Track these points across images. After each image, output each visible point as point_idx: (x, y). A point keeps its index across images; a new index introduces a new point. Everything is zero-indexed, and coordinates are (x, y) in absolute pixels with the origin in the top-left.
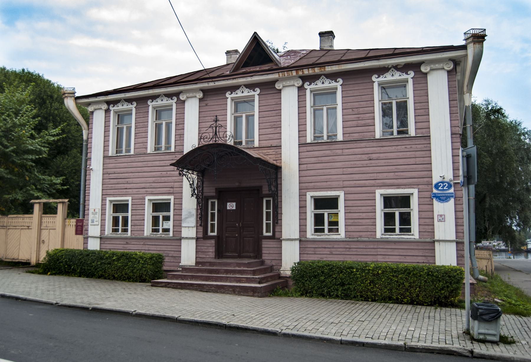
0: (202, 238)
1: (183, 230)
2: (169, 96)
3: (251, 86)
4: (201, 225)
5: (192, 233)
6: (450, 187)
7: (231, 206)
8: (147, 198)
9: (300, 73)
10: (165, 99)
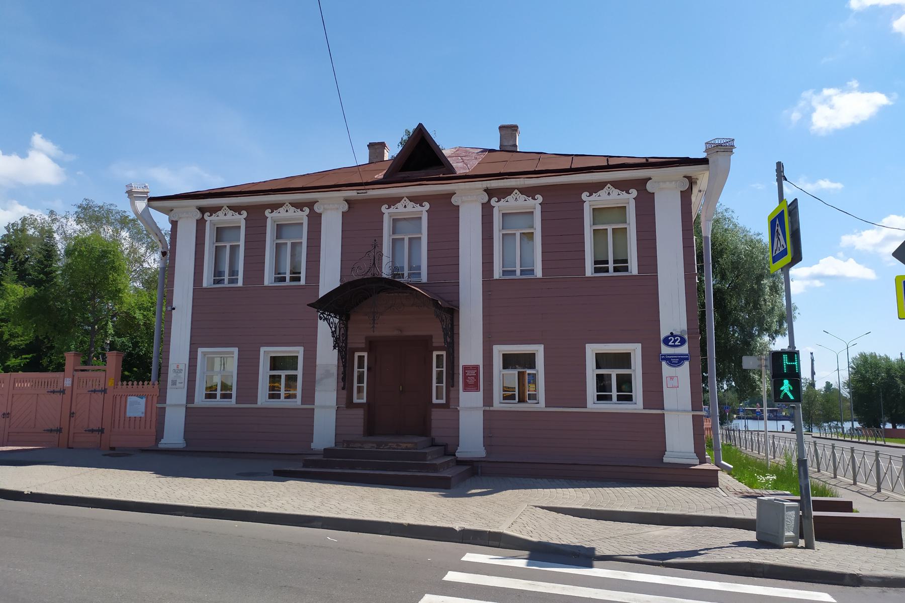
2: (299, 206)
3: (417, 199)
4: (343, 389)
10: (615, 192)
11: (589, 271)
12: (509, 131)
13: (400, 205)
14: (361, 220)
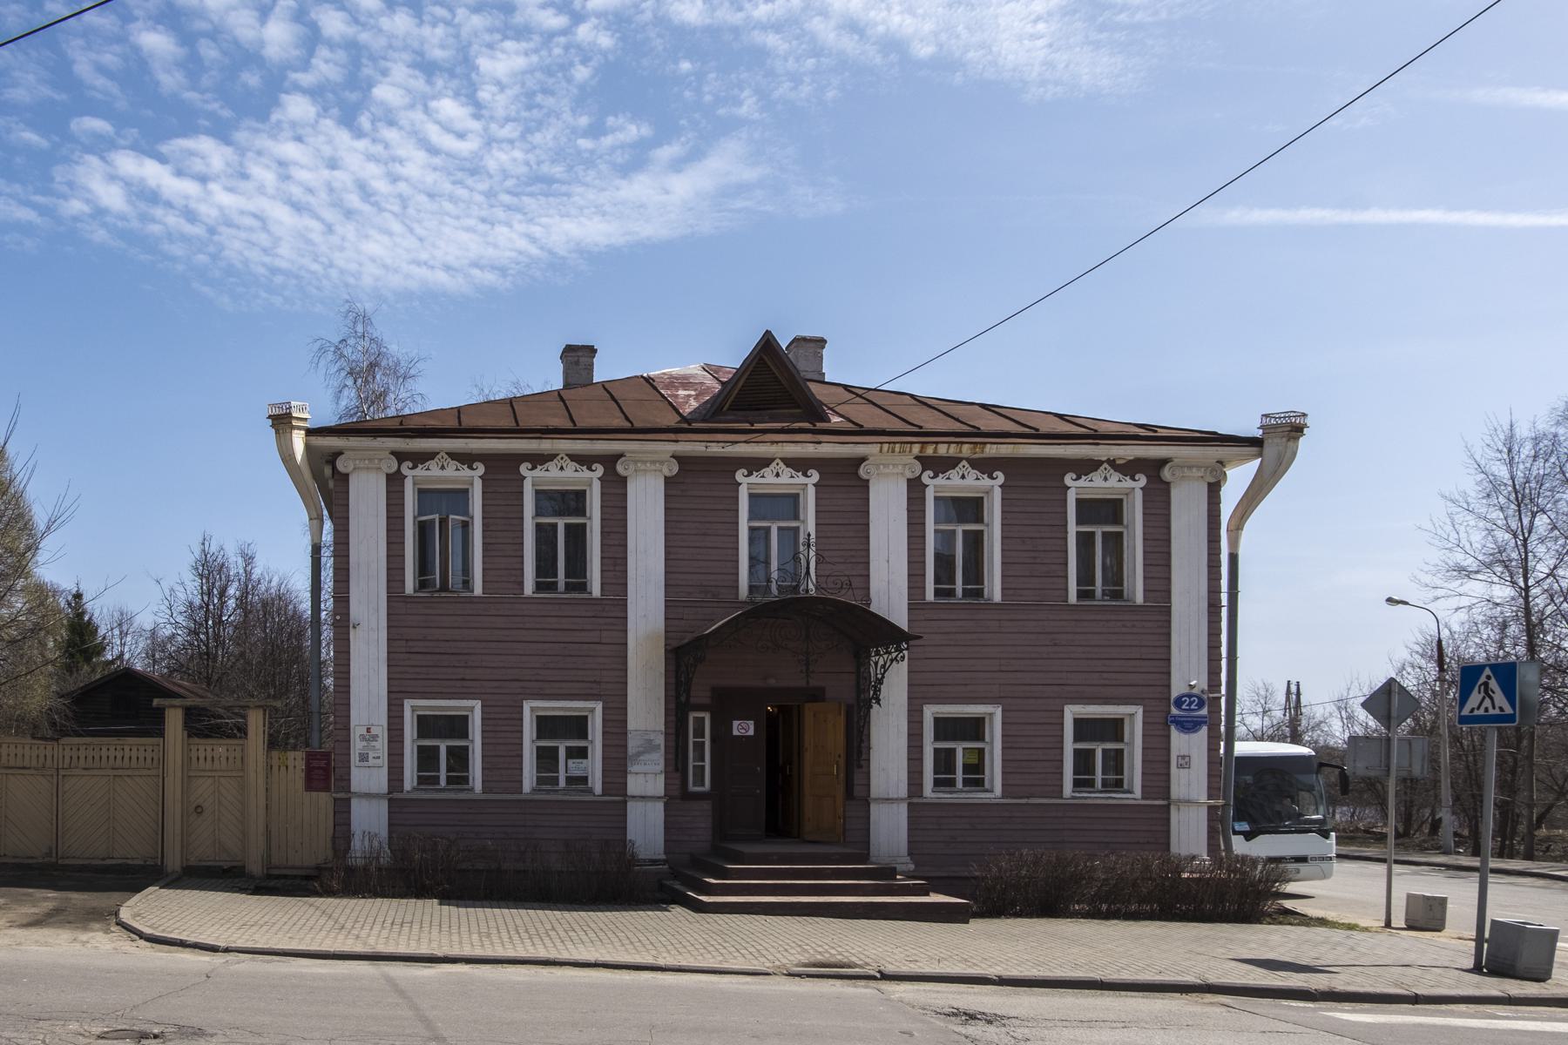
0: (677, 797)
1: (631, 780)
3: (799, 465)
5: (657, 786)
6: (1201, 704)
7: (743, 728)
8: (527, 706)
9: (930, 451)
11: (529, 588)
12: (578, 357)
13: (954, 474)
14: (698, 490)
